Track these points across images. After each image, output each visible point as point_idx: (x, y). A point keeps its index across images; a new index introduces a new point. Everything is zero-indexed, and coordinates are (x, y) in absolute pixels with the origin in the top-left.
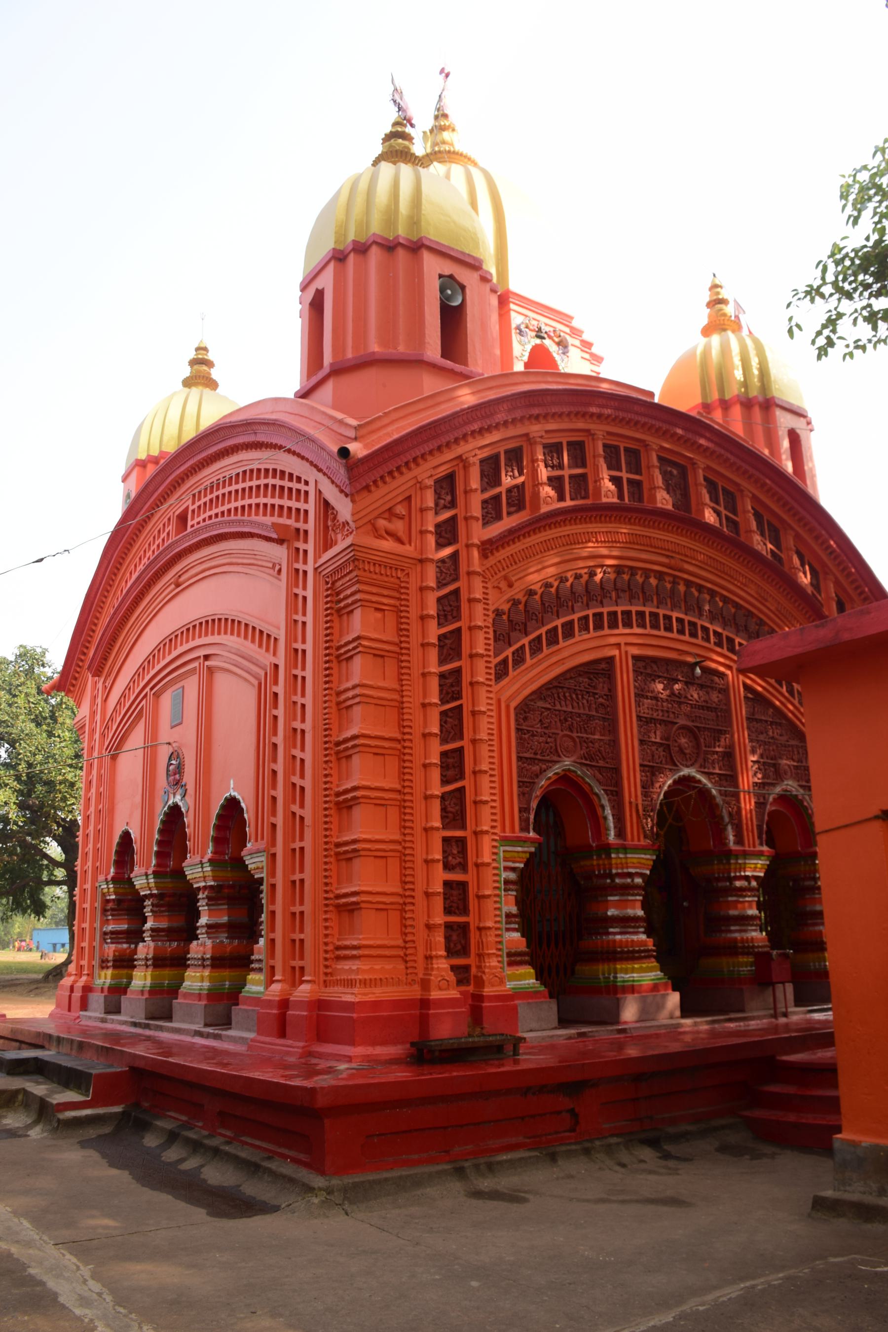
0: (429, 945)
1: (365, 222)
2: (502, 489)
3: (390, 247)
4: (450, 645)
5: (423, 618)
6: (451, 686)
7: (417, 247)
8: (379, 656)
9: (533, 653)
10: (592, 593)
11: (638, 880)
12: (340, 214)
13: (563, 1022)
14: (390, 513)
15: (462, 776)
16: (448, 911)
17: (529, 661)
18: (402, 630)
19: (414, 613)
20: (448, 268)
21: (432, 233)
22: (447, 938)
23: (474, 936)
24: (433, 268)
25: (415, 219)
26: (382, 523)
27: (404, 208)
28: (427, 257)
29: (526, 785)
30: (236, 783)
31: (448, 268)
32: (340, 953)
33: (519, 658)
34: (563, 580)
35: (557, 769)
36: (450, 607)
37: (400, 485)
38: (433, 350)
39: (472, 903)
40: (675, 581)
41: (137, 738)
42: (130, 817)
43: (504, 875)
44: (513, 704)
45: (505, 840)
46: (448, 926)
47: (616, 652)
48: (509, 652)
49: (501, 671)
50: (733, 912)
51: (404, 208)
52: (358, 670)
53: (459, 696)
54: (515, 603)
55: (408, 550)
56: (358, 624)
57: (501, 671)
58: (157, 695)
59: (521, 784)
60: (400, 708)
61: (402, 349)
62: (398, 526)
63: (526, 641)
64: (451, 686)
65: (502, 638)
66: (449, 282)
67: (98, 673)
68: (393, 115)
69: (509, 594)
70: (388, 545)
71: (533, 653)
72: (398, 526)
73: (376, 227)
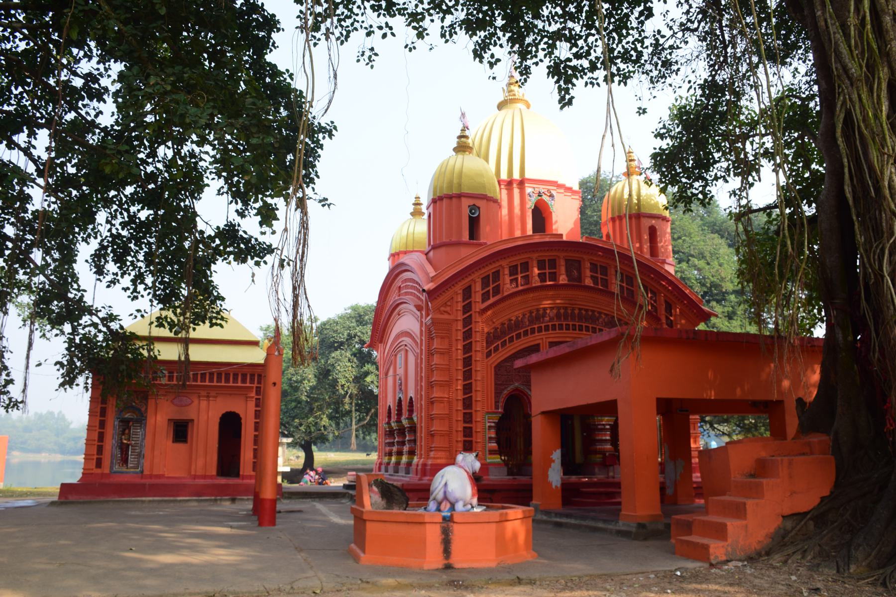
0: (457, 447)
1: (442, 188)
2: (491, 288)
3: (450, 197)
4: (468, 348)
5: (457, 340)
6: (468, 362)
7: (459, 196)
8: (442, 353)
9: (502, 346)
10: (518, 324)
11: (608, 427)
12: (443, 170)
13: (508, 475)
14: (445, 305)
15: (471, 392)
16: (464, 436)
17: (500, 350)
18: (451, 345)
19: (454, 338)
20: (471, 202)
21: (465, 190)
22: (464, 445)
23: (474, 444)
24: (466, 203)
25: (460, 185)
26: (442, 309)
27: (455, 181)
28: (463, 199)
29: (498, 393)
30: (411, 393)
31: (471, 202)
32: (430, 449)
33: (496, 349)
34: (510, 320)
35: (512, 387)
36: (468, 335)
37: (450, 293)
38: (466, 237)
39: (474, 434)
40: (573, 309)
41: (391, 373)
42: (391, 402)
43: (488, 424)
44: (493, 366)
45: (488, 413)
46: (464, 441)
47: (540, 341)
48: (492, 347)
49: (489, 354)
50: (597, 438)
51: (455, 181)
52: (436, 359)
53: (471, 365)
54: (496, 329)
55: (452, 317)
56: (436, 344)
57: (489, 354)
58: (396, 355)
59: (496, 393)
60: (449, 370)
61: (454, 239)
62: (448, 309)
63: (499, 342)
64: (468, 362)
65: (489, 342)
66: (473, 208)
67: (381, 342)
68: (461, 127)
69: (494, 325)
70: (446, 316)
71: (502, 346)
72: (448, 309)
73: (445, 192)
